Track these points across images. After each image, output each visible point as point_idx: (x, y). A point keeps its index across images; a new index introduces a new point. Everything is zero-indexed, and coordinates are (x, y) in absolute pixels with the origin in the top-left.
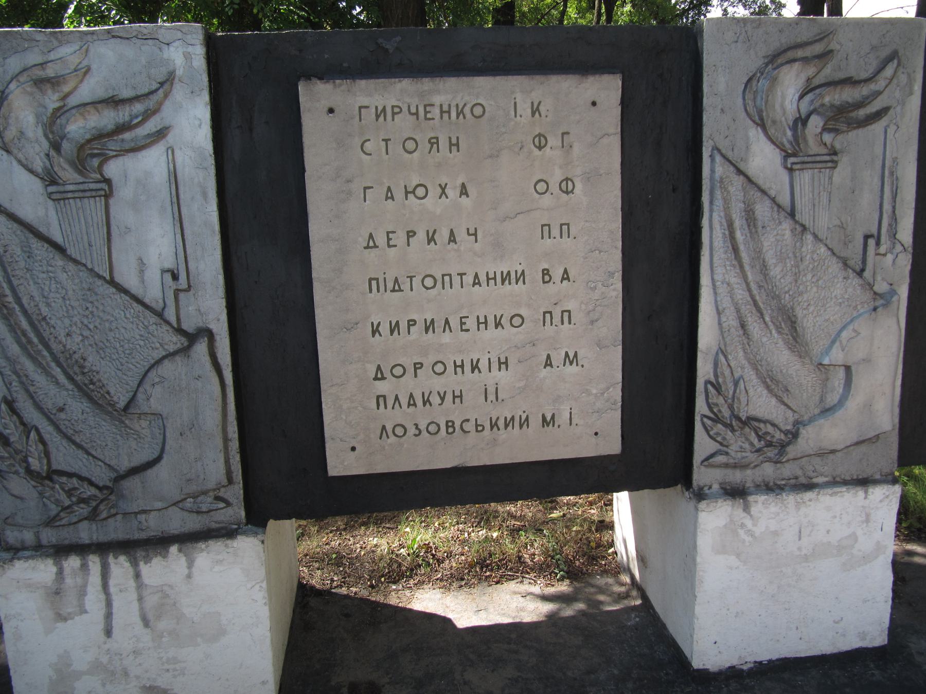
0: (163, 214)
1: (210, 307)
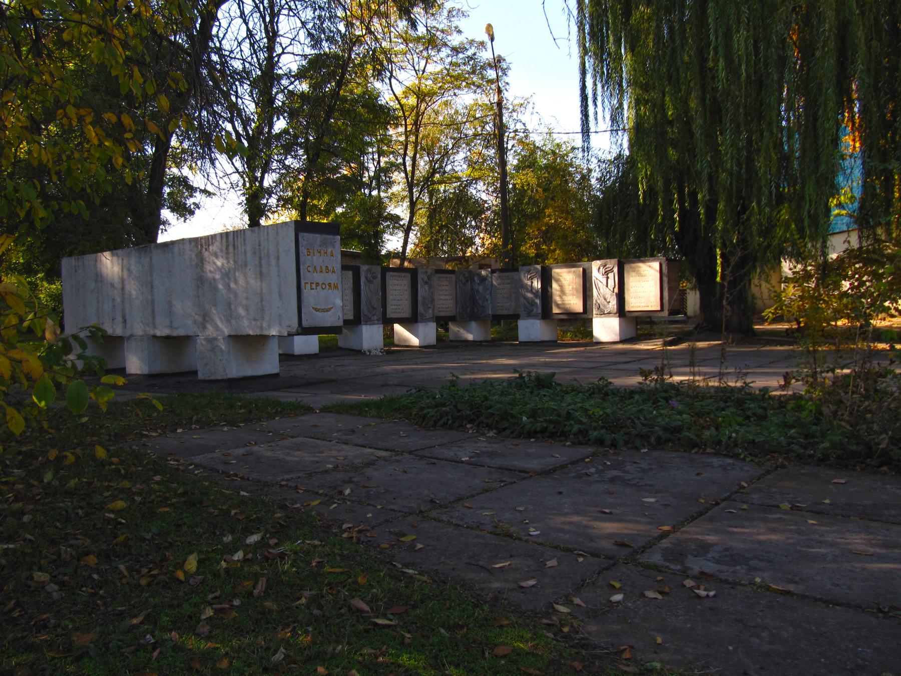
1: (160, 231)
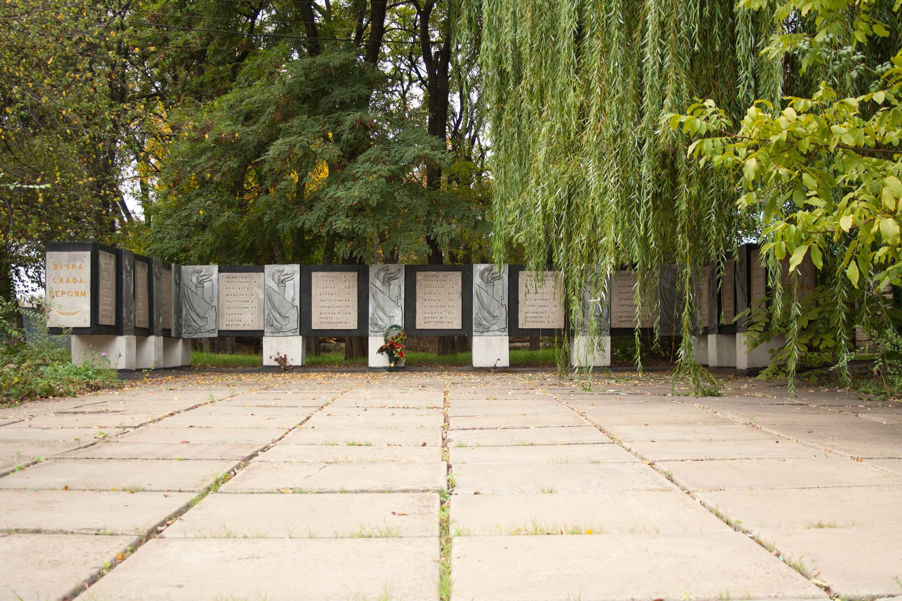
0: (293, 290)
